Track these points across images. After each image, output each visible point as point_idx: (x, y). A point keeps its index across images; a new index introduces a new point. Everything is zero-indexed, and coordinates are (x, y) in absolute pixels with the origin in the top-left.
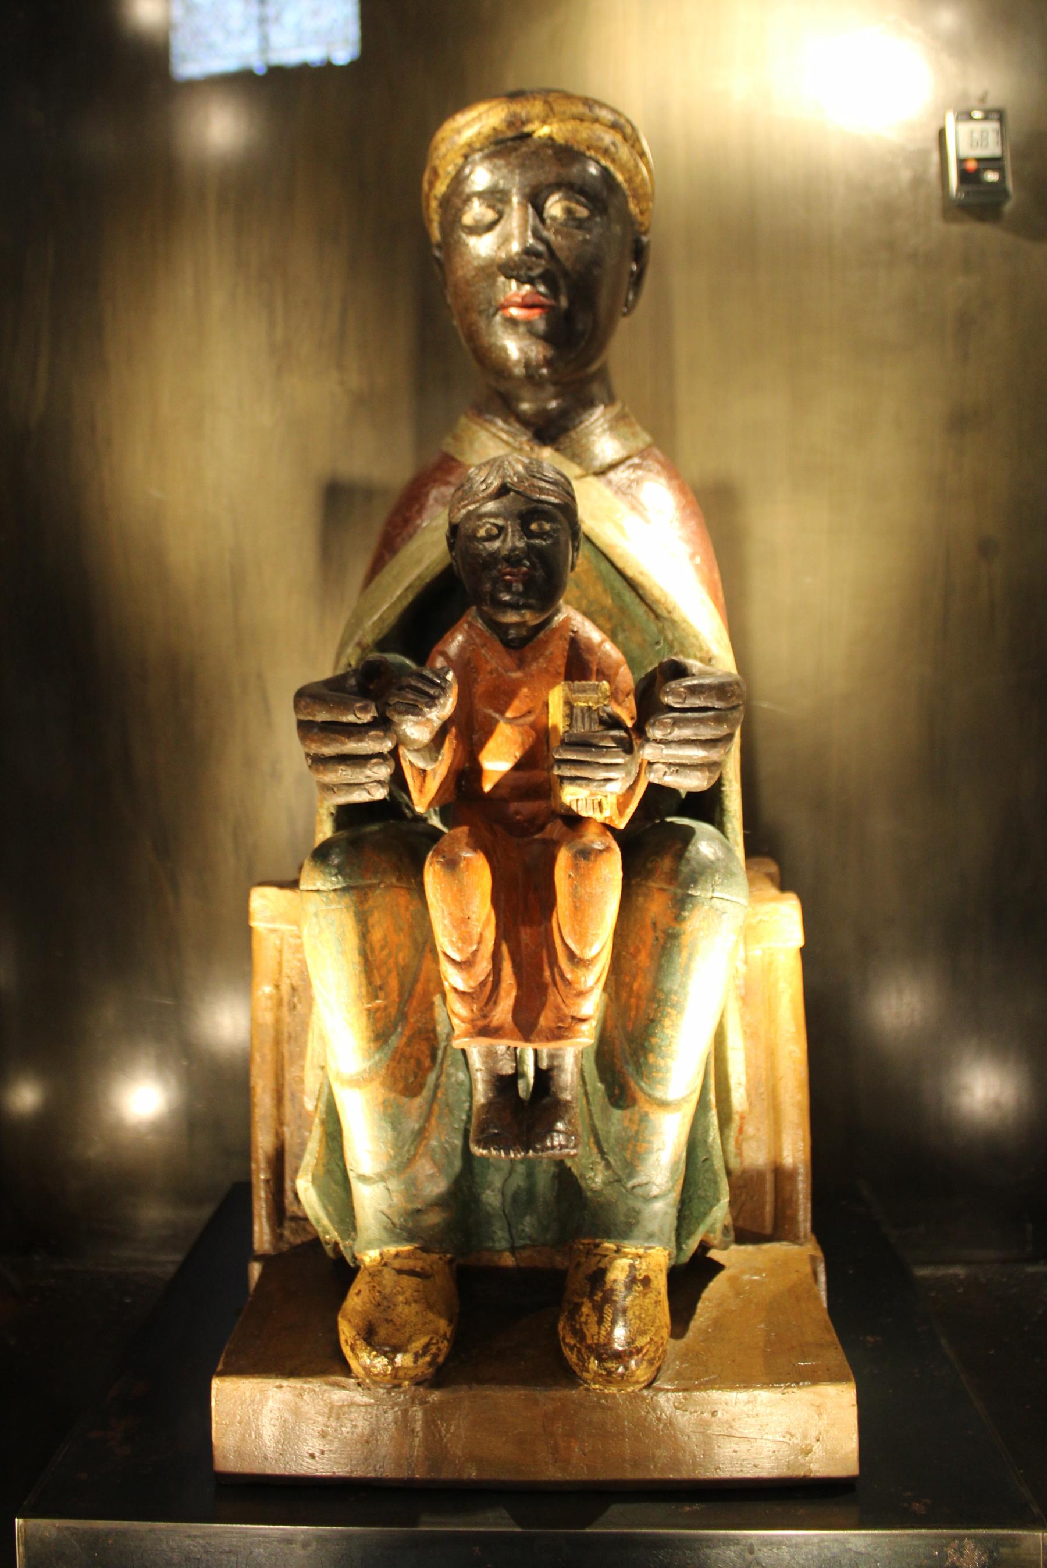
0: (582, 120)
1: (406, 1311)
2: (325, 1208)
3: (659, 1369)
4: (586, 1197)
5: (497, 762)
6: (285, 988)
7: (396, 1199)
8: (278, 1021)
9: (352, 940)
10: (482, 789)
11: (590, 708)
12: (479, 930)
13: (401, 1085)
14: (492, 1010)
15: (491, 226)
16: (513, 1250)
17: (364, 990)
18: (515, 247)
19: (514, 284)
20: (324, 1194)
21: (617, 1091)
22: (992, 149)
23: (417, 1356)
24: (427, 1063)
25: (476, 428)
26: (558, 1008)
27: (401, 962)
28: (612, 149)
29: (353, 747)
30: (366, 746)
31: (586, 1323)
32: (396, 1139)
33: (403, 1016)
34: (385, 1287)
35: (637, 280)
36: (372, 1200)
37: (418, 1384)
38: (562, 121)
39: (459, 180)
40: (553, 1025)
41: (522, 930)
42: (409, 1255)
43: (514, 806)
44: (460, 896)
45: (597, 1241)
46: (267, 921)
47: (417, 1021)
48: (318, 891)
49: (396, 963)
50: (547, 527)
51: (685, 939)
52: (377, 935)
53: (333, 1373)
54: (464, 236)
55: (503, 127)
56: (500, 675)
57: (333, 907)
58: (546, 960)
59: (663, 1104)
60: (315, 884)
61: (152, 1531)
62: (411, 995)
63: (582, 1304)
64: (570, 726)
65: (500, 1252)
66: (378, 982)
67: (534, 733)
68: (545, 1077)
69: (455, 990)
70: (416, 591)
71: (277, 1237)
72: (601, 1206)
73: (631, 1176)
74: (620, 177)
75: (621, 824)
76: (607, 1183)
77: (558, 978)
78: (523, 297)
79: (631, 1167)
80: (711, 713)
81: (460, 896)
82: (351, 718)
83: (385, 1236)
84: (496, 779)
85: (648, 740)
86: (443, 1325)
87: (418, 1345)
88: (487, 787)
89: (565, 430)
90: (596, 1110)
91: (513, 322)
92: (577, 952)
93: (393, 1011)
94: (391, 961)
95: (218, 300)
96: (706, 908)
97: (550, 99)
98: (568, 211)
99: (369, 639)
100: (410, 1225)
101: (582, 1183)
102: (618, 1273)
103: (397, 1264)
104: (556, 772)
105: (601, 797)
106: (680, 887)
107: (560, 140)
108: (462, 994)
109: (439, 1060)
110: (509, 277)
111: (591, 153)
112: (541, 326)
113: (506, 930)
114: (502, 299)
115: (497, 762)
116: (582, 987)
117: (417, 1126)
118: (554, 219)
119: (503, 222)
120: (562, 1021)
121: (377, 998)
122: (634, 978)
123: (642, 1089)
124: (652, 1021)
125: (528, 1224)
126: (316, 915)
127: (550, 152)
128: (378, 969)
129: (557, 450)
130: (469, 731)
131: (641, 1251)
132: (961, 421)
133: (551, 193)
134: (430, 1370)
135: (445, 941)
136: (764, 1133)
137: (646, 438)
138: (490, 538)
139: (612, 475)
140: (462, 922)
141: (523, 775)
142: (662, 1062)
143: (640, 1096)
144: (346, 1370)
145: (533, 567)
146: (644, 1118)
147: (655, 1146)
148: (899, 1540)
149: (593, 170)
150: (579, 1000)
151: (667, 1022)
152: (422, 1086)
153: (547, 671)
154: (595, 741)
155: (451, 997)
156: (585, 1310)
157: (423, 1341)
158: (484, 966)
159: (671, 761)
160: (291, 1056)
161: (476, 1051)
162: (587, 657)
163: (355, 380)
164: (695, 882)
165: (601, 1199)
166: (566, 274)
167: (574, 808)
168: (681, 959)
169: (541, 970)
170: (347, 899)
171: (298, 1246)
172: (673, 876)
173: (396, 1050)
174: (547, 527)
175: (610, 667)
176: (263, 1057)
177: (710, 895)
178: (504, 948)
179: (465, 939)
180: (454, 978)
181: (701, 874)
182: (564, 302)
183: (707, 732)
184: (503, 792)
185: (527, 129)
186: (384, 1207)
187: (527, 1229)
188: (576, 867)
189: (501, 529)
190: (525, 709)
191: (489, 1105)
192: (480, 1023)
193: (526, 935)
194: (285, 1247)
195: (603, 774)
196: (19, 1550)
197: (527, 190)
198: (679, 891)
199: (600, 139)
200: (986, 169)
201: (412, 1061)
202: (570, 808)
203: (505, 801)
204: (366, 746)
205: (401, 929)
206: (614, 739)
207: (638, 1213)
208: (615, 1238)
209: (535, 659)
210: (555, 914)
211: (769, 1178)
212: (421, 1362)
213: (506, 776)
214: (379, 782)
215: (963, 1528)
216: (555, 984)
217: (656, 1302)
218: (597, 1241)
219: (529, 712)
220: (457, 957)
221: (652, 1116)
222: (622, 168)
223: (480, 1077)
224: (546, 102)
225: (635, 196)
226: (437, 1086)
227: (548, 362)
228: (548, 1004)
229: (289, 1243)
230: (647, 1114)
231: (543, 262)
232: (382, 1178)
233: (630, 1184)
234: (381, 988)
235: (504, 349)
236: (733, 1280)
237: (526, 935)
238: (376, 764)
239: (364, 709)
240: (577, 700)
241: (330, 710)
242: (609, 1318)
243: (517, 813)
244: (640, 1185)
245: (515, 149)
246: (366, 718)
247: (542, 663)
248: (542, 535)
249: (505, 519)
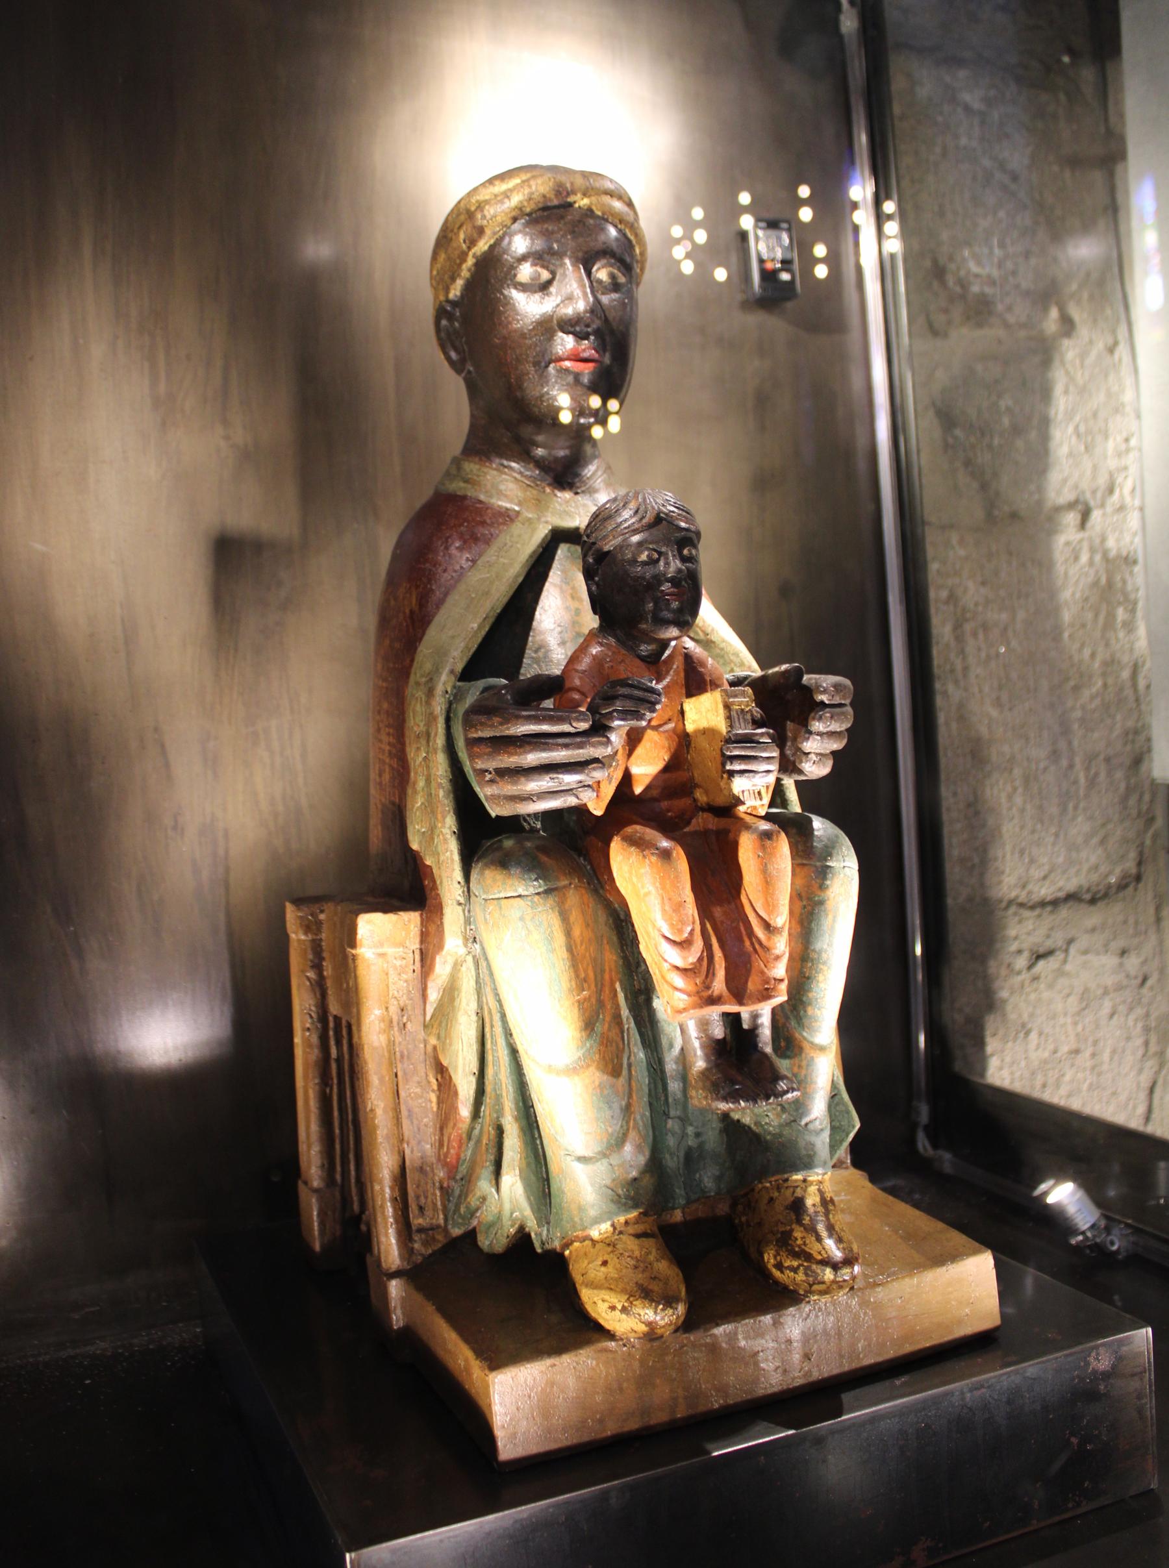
2: (528, 1198)
4: (766, 1142)
6: (394, 1010)
8: (391, 1043)
9: (560, 939)
10: (633, 792)
11: (742, 710)
14: (712, 982)
21: (783, 1044)
26: (763, 973)
31: (805, 1244)
34: (632, 1251)
40: (761, 988)
42: (637, 1221)
43: (665, 804)
45: (786, 1176)
46: (376, 946)
48: (519, 896)
51: (830, 905)
53: (598, 1341)
58: (744, 932)
60: (516, 891)
62: (602, 985)
63: (792, 1230)
64: (731, 726)
70: (491, 620)
72: (783, 1145)
73: (802, 1116)
77: (757, 946)
83: (613, 1207)
84: (647, 781)
85: (810, 733)
93: (594, 1000)
95: (97, 351)
98: (612, 276)
106: (819, 861)
120: (768, 983)
121: (583, 990)
123: (805, 1038)
124: (808, 978)
126: (522, 919)
141: (667, 775)
142: (818, 1012)
143: (805, 1045)
148: (1069, 1359)
151: (821, 977)
158: (699, 944)
160: (405, 1073)
163: (240, 436)
164: (830, 855)
169: (742, 941)
170: (551, 901)
171: (430, 1255)
177: (842, 865)
178: (708, 926)
181: (833, 848)
184: (655, 793)
186: (608, 1182)
188: (763, 848)
192: (705, 994)
194: (419, 1259)
198: (818, 864)
207: (813, 1145)
208: (803, 1169)
210: (743, 891)
213: (656, 777)
215: (990, 1371)
218: (786, 1176)
226: (630, 1065)
228: (753, 970)
229: (421, 1255)
230: (812, 1058)
232: (604, 1155)
233: (803, 1123)
238: (594, 769)
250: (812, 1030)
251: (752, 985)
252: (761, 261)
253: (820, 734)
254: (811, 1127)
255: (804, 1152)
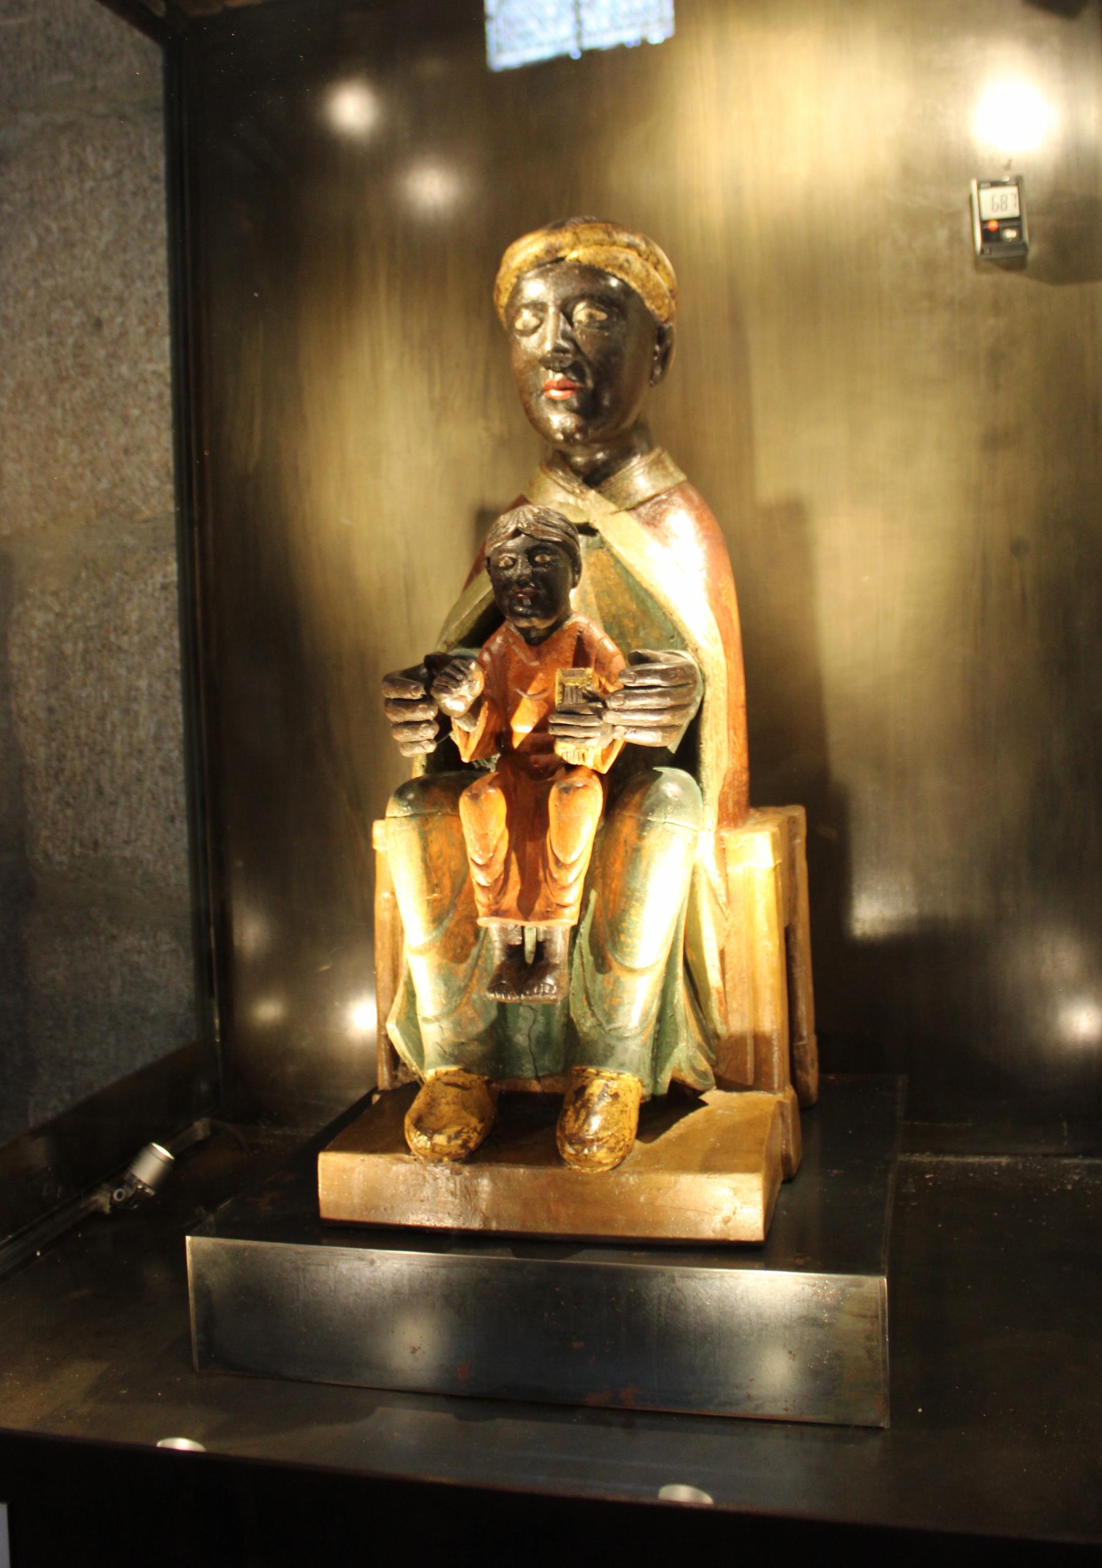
0: (602, 245)
1: (446, 1109)
2: (407, 1044)
3: (623, 1158)
5: (522, 727)
7: (448, 1034)
12: (495, 842)
13: (451, 955)
15: (535, 329)
16: (538, 1078)
17: (425, 887)
18: (548, 347)
19: (551, 373)
20: (405, 1033)
22: (1012, 211)
23: (450, 1139)
24: (472, 939)
25: (543, 476)
26: (547, 898)
27: (453, 868)
28: (626, 265)
29: (410, 716)
30: (419, 715)
32: (447, 992)
33: (454, 905)
35: (665, 357)
36: (435, 1034)
37: (455, 1160)
38: (586, 247)
39: (517, 291)
41: (528, 843)
42: (455, 1074)
43: (533, 758)
44: (482, 819)
47: (464, 910)
49: (449, 868)
50: (548, 558)
51: (645, 852)
52: (434, 849)
54: (518, 337)
55: (542, 254)
56: (524, 664)
57: (404, 828)
59: (631, 971)
61: (273, 1248)
62: (460, 892)
65: (529, 1079)
66: (436, 882)
67: (546, 706)
68: (541, 947)
69: (479, 884)
71: (394, 1078)
72: (588, 1043)
74: (634, 285)
75: (604, 770)
76: (593, 1027)
78: (558, 382)
79: (610, 1017)
80: (659, 689)
81: (482, 819)
82: (408, 696)
83: (439, 1059)
86: (474, 1122)
87: (452, 1130)
88: (516, 744)
89: (607, 476)
90: (588, 975)
91: (553, 402)
92: (561, 858)
93: (446, 902)
94: (445, 867)
95: (389, 366)
96: (660, 829)
97: (578, 231)
98: (591, 316)
99: (453, 638)
100: (456, 1053)
101: (578, 1028)
102: (596, 1087)
103: (445, 1079)
104: (551, 733)
105: (589, 749)
107: (585, 261)
108: (483, 887)
109: (481, 938)
110: (548, 368)
111: (609, 270)
112: (575, 403)
113: (516, 845)
114: (543, 384)
115: (522, 727)
116: (564, 883)
117: (463, 984)
118: (580, 322)
119: (543, 326)
121: (434, 892)
122: (612, 880)
123: (616, 960)
124: (623, 911)
125: (547, 1061)
126: (393, 834)
127: (577, 271)
128: (435, 872)
129: (600, 492)
130: (498, 702)
131: (614, 1075)
132: (994, 441)
133: (577, 303)
134: (462, 1151)
135: (474, 853)
136: (747, 1007)
137: (681, 477)
138: (507, 567)
139: (642, 510)
140: (483, 837)
141: (535, 735)
142: (629, 940)
143: (614, 964)
144: (408, 1150)
145: (537, 587)
146: (617, 980)
147: (626, 1001)
149: (614, 283)
150: (564, 893)
151: (633, 912)
152: (467, 956)
153: (557, 661)
154: (578, 710)
155: (477, 890)
156: (570, 1113)
157: (457, 1128)
158: (498, 868)
159: (630, 724)
161: (492, 926)
162: (588, 650)
164: (653, 811)
165: (588, 1038)
166: (589, 363)
167: (565, 758)
168: (642, 866)
169: (537, 872)
170: (414, 823)
172: (640, 806)
173: (447, 930)
174: (548, 558)
175: (606, 657)
176: (383, 944)
177: (663, 820)
179: (485, 848)
180: (479, 877)
181: (657, 806)
182: (590, 383)
183: (667, 702)
185: (561, 254)
186: (439, 1040)
187: (547, 1063)
188: (560, 799)
189: (515, 561)
190: (541, 688)
191: (502, 966)
192: (494, 907)
193: (530, 847)
194: (398, 1084)
195: (583, 734)
196: (189, 1257)
197: (559, 302)
198: (642, 818)
199: (616, 258)
200: (1005, 228)
201: (460, 938)
202: (561, 759)
203: (528, 754)
204: (419, 715)
205: (453, 845)
206: (591, 709)
209: (549, 652)
211: (750, 1042)
212: (453, 1143)
213: (528, 736)
214: (429, 740)
216: (546, 880)
217: (622, 1111)
219: (544, 691)
220: (480, 861)
221: (622, 979)
222: (636, 277)
223: (497, 945)
224: (575, 233)
225: (650, 297)
226: (479, 957)
227: (579, 429)
230: (618, 977)
231: (569, 356)
233: (607, 1029)
234: (437, 885)
235: (548, 420)
236: (711, 1112)
237: (530, 847)
239: (416, 689)
240: (568, 681)
241: (396, 691)
242: (582, 1117)
243: (536, 762)
244: (615, 1029)
245: (551, 270)
246: (418, 695)
247: (555, 656)
248: (544, 564)
249: (517, 554)
250: (624, 955)
251: (539, 907)
252: (984, 223)
253: (614, 710)
254: (613, 1033)
255: (601, 1051)
